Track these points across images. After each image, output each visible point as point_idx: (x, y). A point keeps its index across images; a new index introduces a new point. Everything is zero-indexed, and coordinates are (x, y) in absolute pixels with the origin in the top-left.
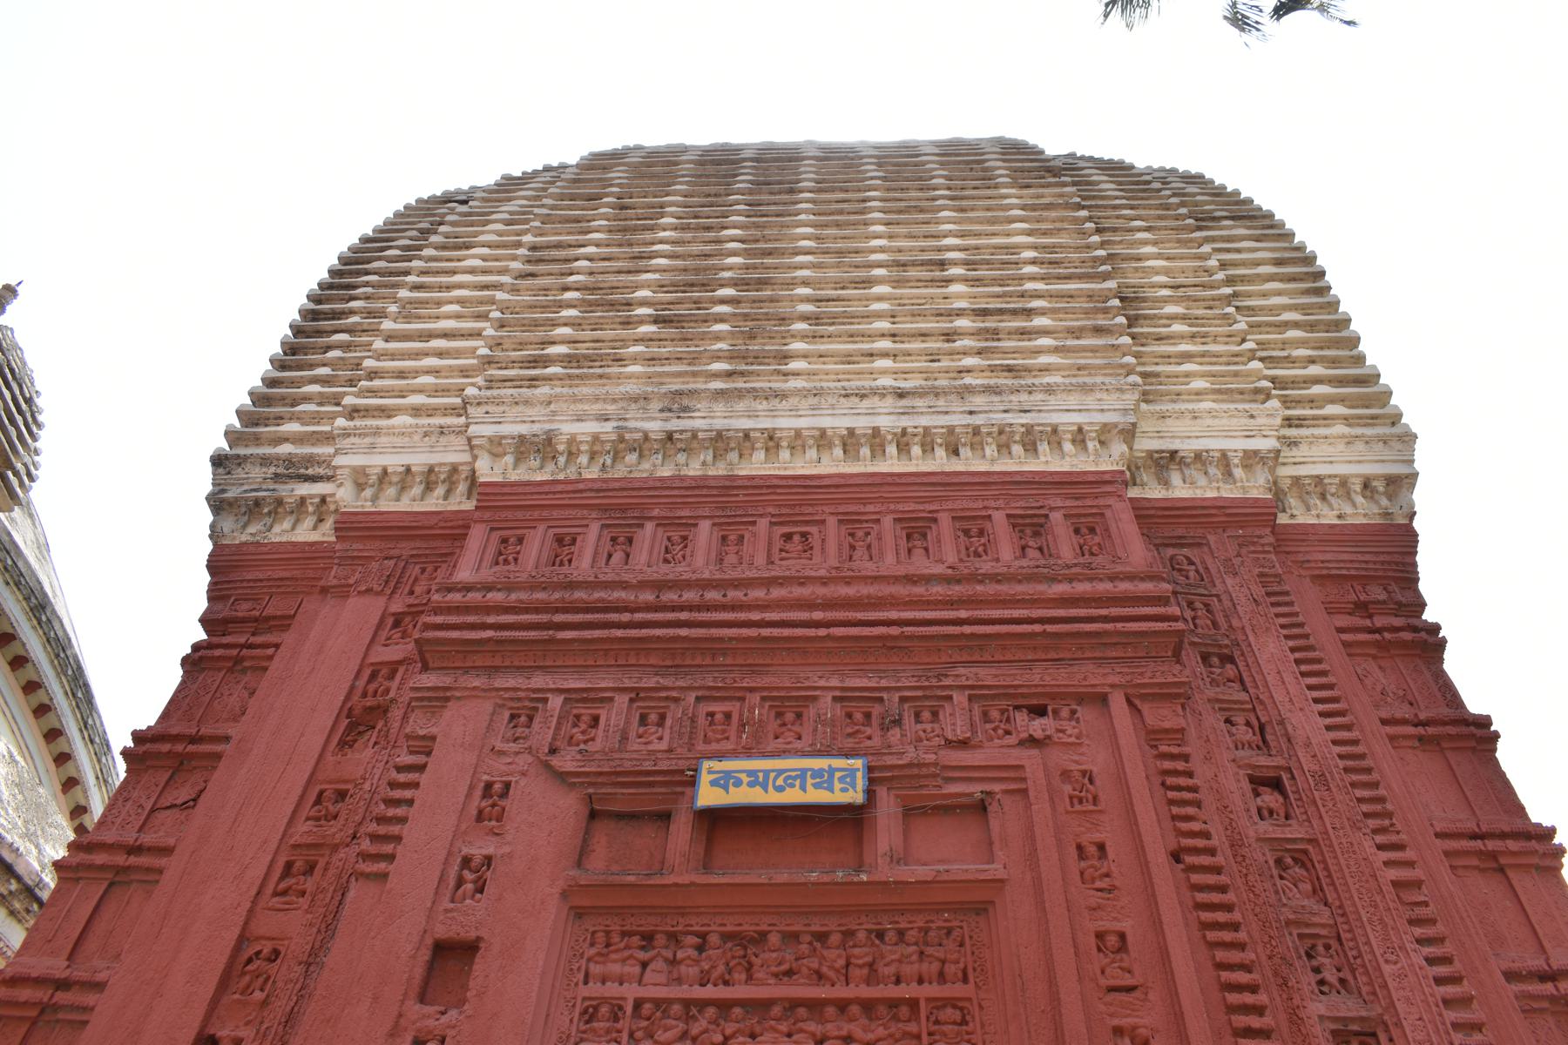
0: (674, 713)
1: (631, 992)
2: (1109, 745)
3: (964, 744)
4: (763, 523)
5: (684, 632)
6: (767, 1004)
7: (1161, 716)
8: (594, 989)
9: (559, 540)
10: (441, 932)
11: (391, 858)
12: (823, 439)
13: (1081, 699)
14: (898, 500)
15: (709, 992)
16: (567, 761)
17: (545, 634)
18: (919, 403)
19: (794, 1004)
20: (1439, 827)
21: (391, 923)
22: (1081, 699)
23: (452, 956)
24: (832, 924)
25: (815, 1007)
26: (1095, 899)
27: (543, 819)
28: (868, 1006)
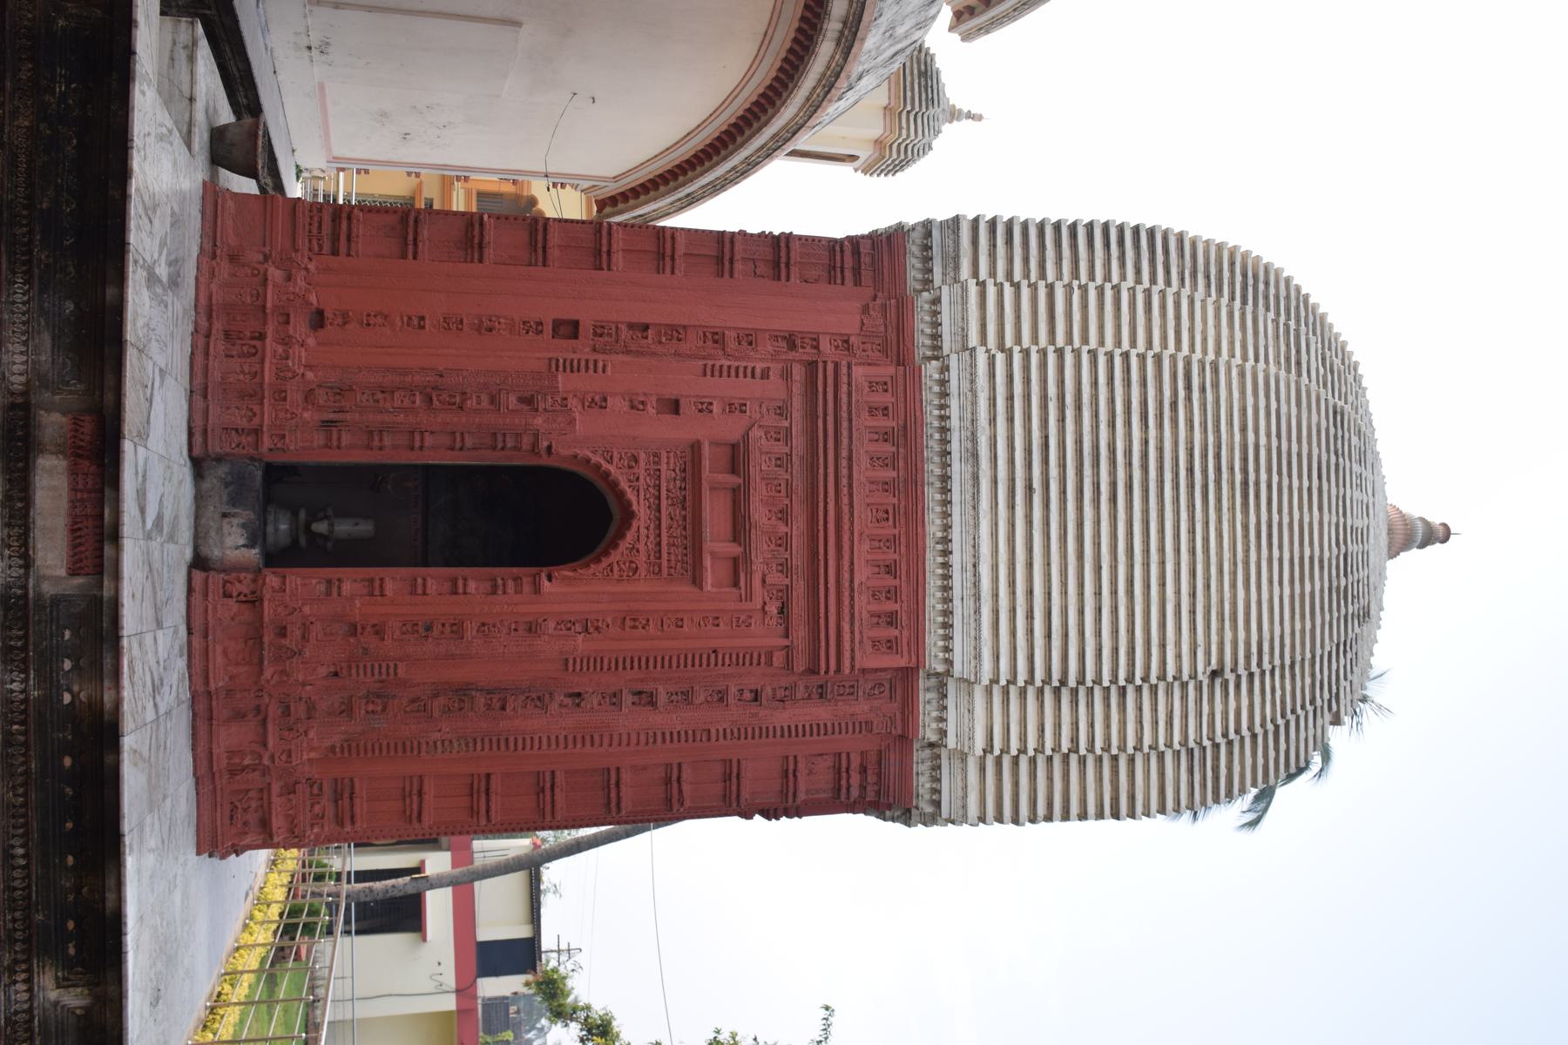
0: (781, 471)
1: (664, 467)
2: (764, 635)
3: (764, 581)
5: (821, 471)
6: (659, 511)
7: (779, 659)
8: (664, 455)
9: (886, 408)
10: (682, 402)
12: (947, 528)
13: (787, 629)
16: (756, 433)
17: (821, 414)
19: (659, 519)
20: (743, 763)
21: (684, 380)
22: (787, 629)
23: (674, 407)
24: (689, 532)
25: (659, 527)
28: (659, 544)
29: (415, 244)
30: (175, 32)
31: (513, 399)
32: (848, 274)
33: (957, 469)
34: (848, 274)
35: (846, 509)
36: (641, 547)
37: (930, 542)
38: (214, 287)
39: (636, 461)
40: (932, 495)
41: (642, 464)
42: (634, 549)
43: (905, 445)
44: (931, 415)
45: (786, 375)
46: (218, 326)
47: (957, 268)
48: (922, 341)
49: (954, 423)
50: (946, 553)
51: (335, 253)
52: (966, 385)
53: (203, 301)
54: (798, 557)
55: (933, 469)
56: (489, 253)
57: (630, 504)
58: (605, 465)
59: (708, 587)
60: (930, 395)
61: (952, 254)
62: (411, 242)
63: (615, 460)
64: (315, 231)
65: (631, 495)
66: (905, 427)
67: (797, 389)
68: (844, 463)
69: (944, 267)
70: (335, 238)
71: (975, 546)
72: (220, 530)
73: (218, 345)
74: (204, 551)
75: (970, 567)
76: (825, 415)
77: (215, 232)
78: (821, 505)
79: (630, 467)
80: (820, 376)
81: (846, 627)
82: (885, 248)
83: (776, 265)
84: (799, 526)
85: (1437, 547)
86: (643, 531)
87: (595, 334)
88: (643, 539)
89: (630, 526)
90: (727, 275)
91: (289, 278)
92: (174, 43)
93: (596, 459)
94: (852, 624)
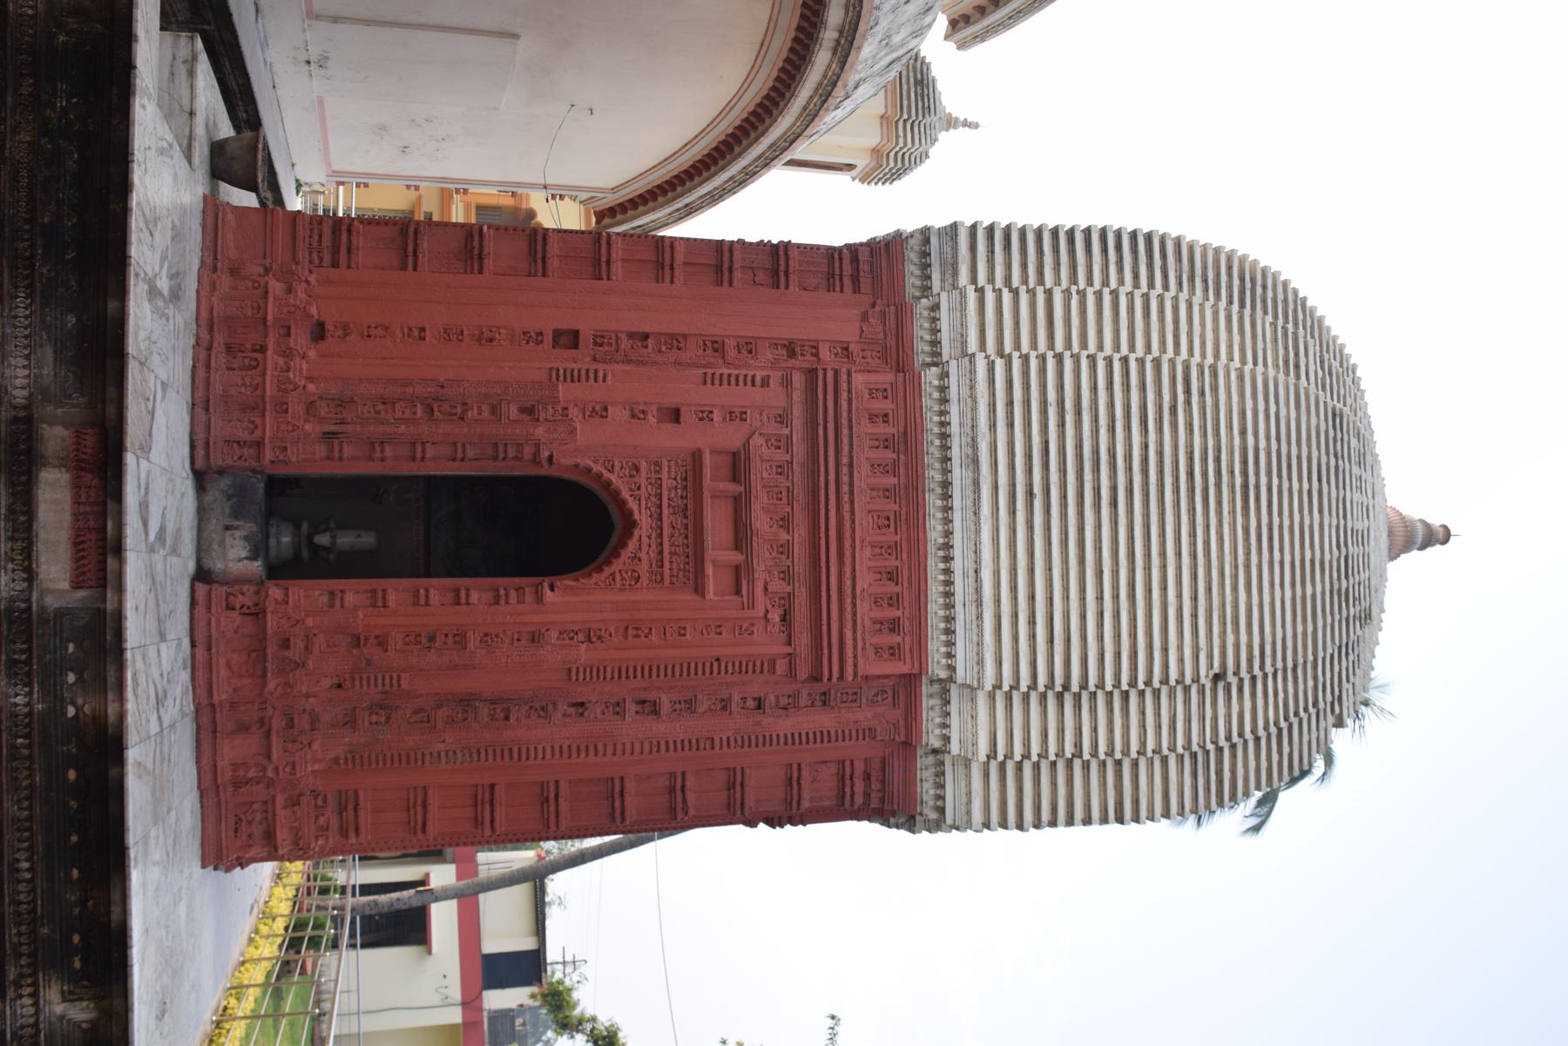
0: (782, 479)
2: (767, 643)
3: (766, 589)
4: (896, 507)
7: (781, 666)
8: (665, 464)
9: (886, 415)
11: (1118, 234)
12: (948, 534)
13: (790, 636)
14: (910, 568)
15: (665, 501)
16: (757, 441)
18: (971, 580)
21: (685, 389)
22: (790, 636)
23: (675, 415)
24: (690, 541)
26: (699, 628)
27: (730, 437)
30: (175, 47)
31: (514, 410)
32: (847, 282)
33: (958, 475)
34: (847, 282)
35: (847, 516)
36: (643, 555)
37: (931, 548)
38: (215, 300)
39: (638, 471)
40: (933, 501)
41: (643, 473)
42: (636, 558)
44: (931, 421)
45: (787, 383)
46: (219, 339)
48: (921, 348)
49: (954, 429)
50: (948, 559)
51: (335, 265)
52: (965, 391)
53: (204, 314)
55: (933, 475)
56: (489, 264)
57: (631, 513)
58: (606, 474)
59: (710, 595)
60: (929, 401)
61: (950, 261)
63: (617, 469)
64: (315, 244)
65: (632, 505)
66: (905, 433)
67: (798, 396)
69: (943, 274)
72: (222, 543)
73: (219, 358)
74: (207, 564)
75: (971, 573)
79: (631, 476)
80: (820, 383)
81: (849, 634)
82: (884, 255)
84: (799, 536)
86: (645, 540)
87: (595, 344)
88: (645, 548)
89: (631, 535)
90: (726, 283)
93: (597, 468)
94: (855, 631)
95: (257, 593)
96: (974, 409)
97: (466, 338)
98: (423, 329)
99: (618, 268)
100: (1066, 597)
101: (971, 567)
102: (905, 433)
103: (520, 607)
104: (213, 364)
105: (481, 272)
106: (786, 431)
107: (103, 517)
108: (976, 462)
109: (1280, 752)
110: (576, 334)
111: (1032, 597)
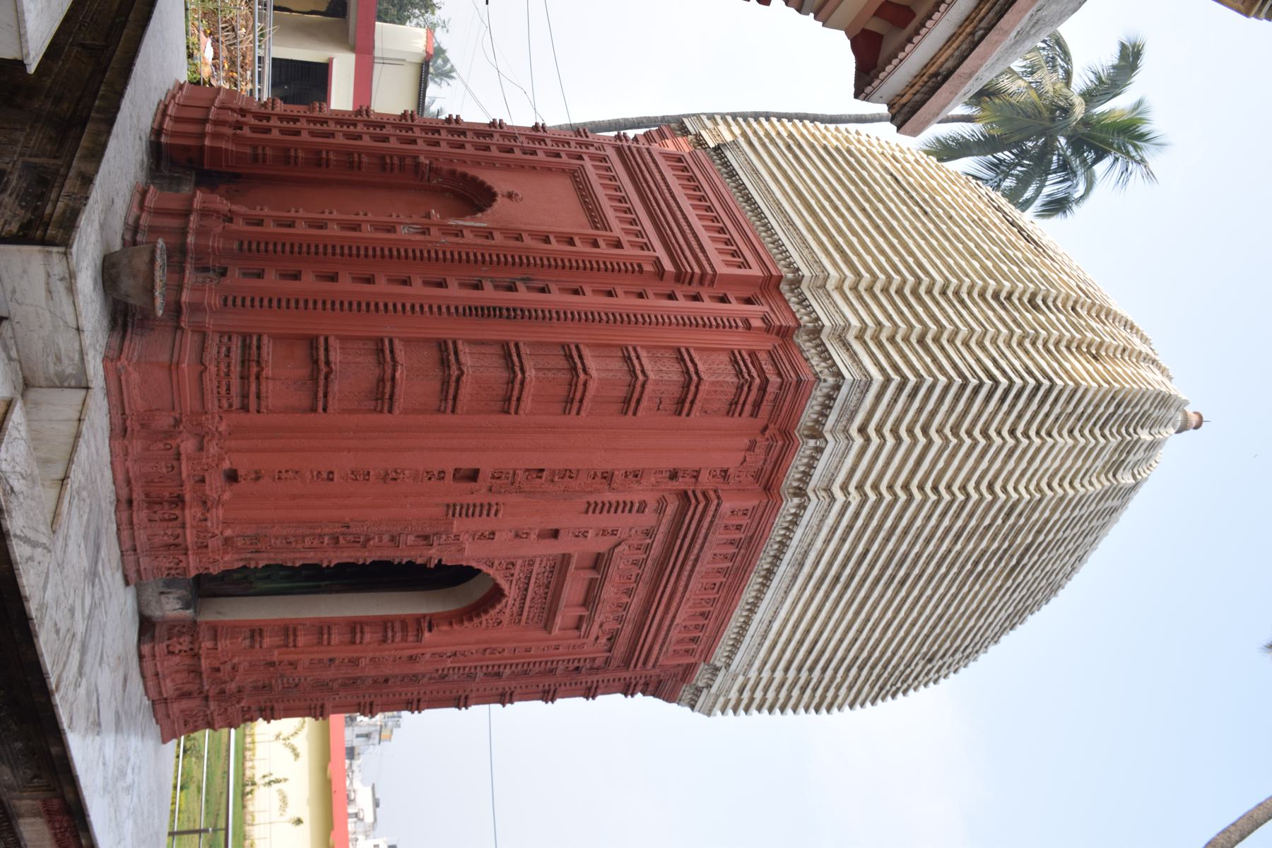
3: (601, 626)
12: (758, 599)
18: (764, 626)
29: (325, 395)
30: (47, 263)
31: (411, 538)
32: (748, 408)
33: (783, 569)
34: (748, 408)
35: (681, 589)
37: (742, 603)
38: (129, 464)
40: (755, 580)
41: (518, 567)
43: (747, 549)
44: (777, 533)
45: (661, 511)
46: (138, 495)
47: (851, 419)
48: (792, 477)
49: (794, 542)
50: (752, 611)
51: (245, 408)
52: (815, 521)
53: (121, 477)
54: (633, 612)
55: (764, 563)
56: (400, 403)
59: (556, 631)
60: (781, 520)
61: (851, 408)
62: (321, 394)
64: (223, 392)
66: (751, 537)
67: (666, 520)
68: (690, 563)
69: (840, 416)
70: (245, 396)
71: (776, 613)
72: (159, 602)
73: (141, 515)
74: (148, 612)
75: (766, 622)
76: (685, 537)
77: (122, 403)
78: (661, 589)
80: (690, 513)
81: (657, 648)
82: (792, 389)
83: (681, 402)
84: (636, 603)
85: (1190, 433)
87: (493, 477)
90: (630, 413)
91: (201, 448)
92: (48, 275)
94: (662, 646)
95: (191, 643)
96: (816, 534)
97: (372, 478)
98: (332, 473)
99: (527, 403)
100: (834, 630)
101: (767, 618)
102: (751, 537)
103: (404, 645)
104: (135, 520)
105: (390, 411)
106: (649, 541)
107: (77, 837)
108: (801, 565)
109: (1005, 462)
110: (477, 471)
111: (807, 632)
